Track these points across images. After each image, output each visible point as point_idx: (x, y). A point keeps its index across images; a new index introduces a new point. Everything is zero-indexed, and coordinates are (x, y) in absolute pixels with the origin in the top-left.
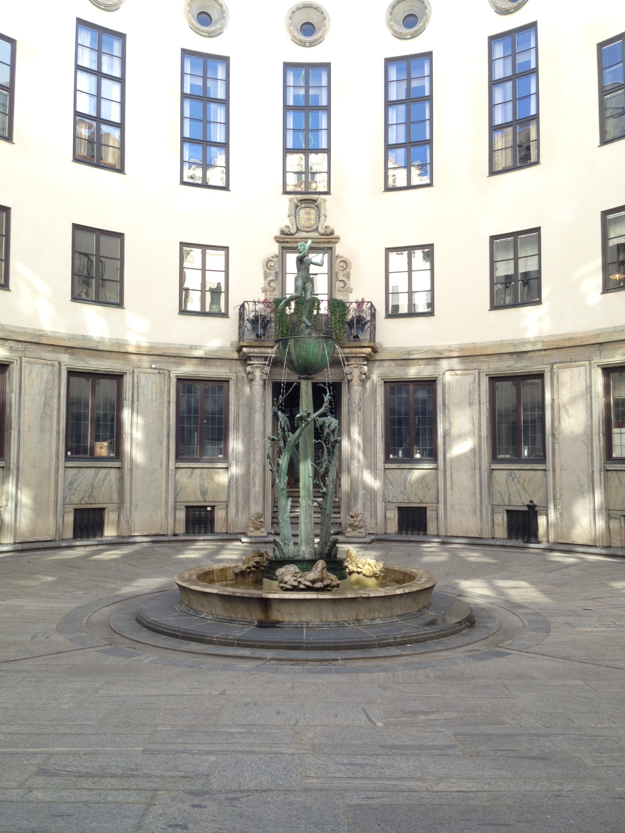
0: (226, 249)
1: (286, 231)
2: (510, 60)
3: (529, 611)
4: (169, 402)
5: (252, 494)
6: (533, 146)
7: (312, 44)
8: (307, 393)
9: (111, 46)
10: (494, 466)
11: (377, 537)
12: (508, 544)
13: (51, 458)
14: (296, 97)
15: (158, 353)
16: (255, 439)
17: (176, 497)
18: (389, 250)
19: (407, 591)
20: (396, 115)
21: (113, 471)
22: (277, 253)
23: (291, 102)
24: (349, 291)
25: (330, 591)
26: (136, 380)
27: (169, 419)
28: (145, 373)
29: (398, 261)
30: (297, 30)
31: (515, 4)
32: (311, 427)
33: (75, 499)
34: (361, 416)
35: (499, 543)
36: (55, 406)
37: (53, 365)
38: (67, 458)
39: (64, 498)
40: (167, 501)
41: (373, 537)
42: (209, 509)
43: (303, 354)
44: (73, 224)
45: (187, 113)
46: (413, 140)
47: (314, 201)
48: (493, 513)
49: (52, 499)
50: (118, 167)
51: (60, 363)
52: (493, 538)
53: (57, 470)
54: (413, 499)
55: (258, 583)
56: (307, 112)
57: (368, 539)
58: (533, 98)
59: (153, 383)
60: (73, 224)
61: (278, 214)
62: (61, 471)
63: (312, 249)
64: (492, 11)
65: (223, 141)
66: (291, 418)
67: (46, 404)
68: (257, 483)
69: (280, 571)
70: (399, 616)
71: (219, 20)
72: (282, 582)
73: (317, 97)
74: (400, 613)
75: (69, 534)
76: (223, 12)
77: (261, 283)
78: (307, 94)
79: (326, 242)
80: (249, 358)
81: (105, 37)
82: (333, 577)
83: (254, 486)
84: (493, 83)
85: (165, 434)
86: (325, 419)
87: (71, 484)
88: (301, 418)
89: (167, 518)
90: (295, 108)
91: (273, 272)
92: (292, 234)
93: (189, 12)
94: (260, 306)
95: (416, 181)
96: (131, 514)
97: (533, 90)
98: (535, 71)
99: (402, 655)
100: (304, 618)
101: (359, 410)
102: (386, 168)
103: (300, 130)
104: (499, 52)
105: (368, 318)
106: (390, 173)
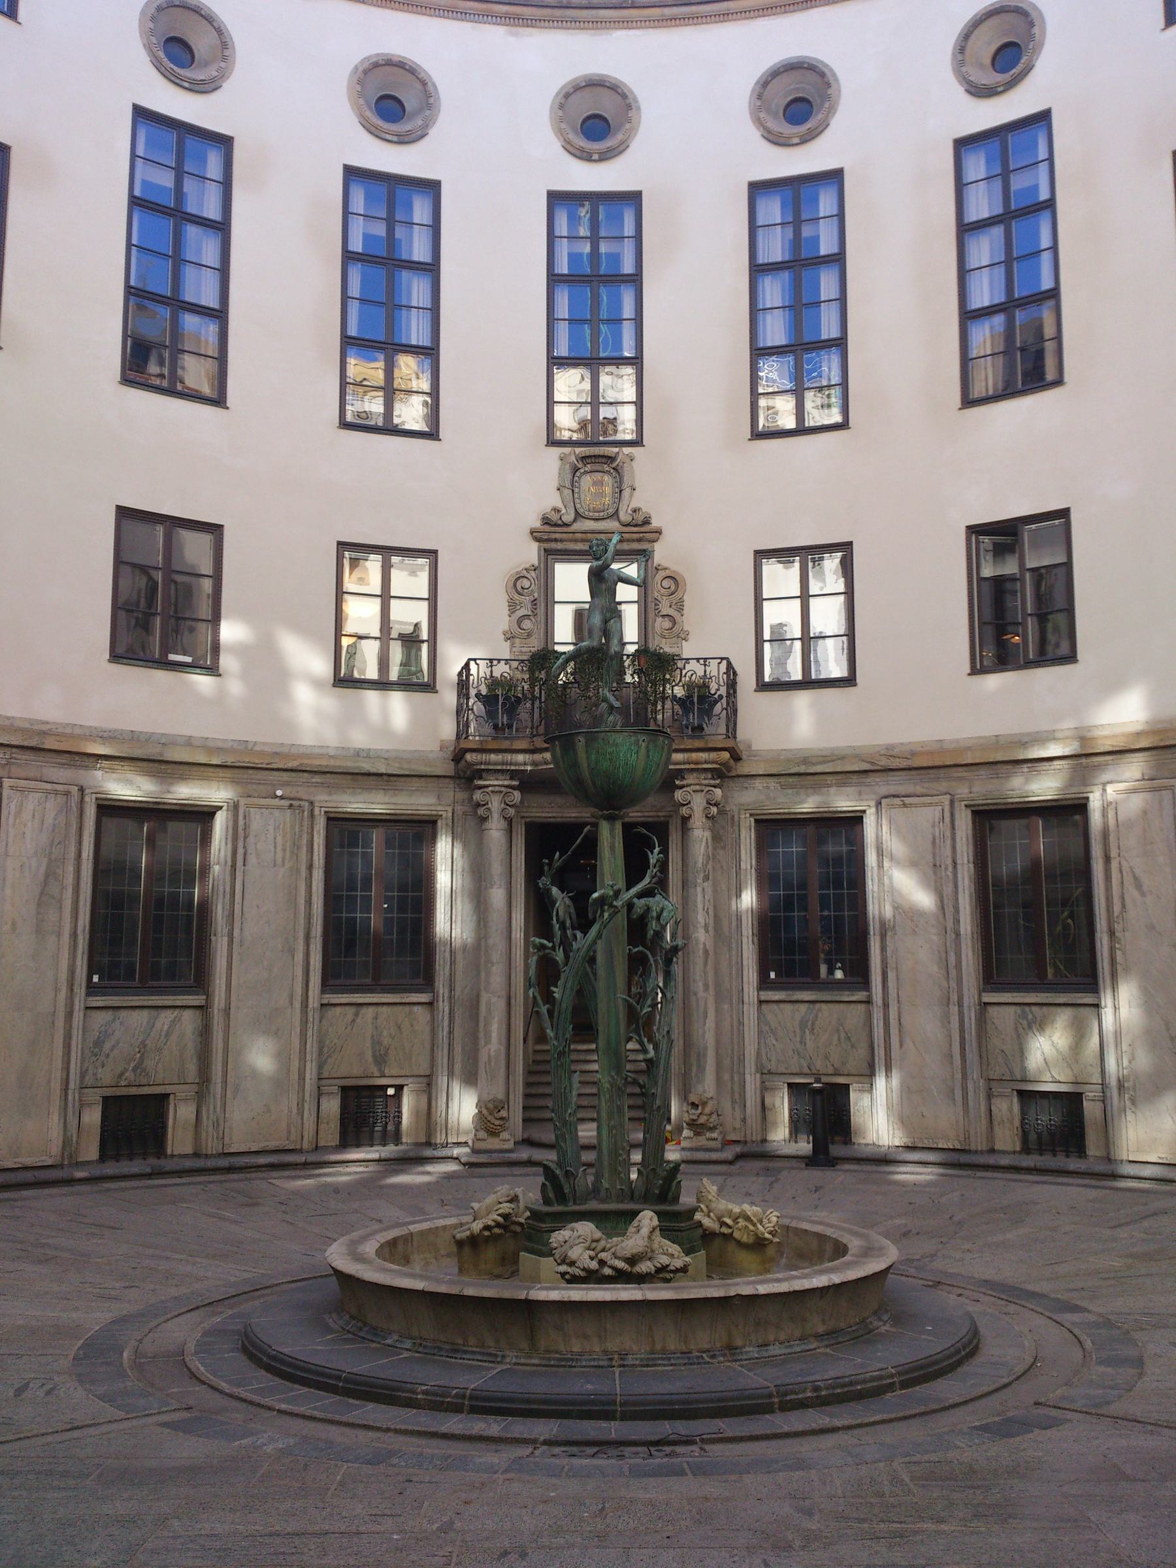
0: (431, 554)
1: (555, 517)
2: (998, 184)
3: (1092, 1318)
4: (310, 867)
5: (483, 1057)
6: (1049, 346)
7: (605, 156)
8: (612, 848)
9: (203, 161)
10: (988, 998)
11: (746, 1149)
12: (1025, 1164)
13: (57, 990)
14: (573, 258)
15: (290, 765)
16: (491, 942)
17: (320, 1067)
18: (761, 555)
19: (837, 1279)
20: (774, 291)
21: (187, 1015)
22: (536, 563)
23: (563, 268)
24: (683, 636)
25: (668, 1281)
26: (241, 822)
27: (309, 902)
28: (260, 807)
29: (781, 578)
30: (574, 129)
31: (1007, 77)
32: (621, 920)
33: (106, 1075)
34: (709, 891)
35: (1004, 1161)
36: (70, 879)
37: (67, 794)
38: (91, 989)
39: (83, 1075)
40: (302, 1078)
41: (738, 1149)
42: (391, 1091)
43: (605, 765)
44: (119, 508)
45: (355, 290)
46: (806, 340)
47: (611, 459)
48: (989, 1096)
49: (58, 1075)
50: (206, 390)
51: (82, 790)
52: (992, 1151)
53: (69, 1015)
54: (819, 1065)
55: (509, 1266)
56: (596, 282)
57: (728, 1154)
58: (1046, 257)
59: (276, 828)
60: (119, 508)
61: (537, 487)
62: (78, 1015)
63: (621, 555)
64: (959, 90)
65: (426, 342)
66: (580, 899)
67: (50, 876)
68: (494, 1035)
69: (557, 1237)
70: (817, 1336)
71: (420, 111)
72: (563, 1262)
73: (616, 258)
74: (821, 1329)
75: (91, 1152)
76: (428, 95)
77: (502, 621)
78: (595, 253)
79: (640, 537)
80: (480, 774)
81: (191, 143)
82: (675, 1249)
83: (488, 1042)
84: (965, 229)
85: (301, 935)
86: (650, 901)
87: (98, 1043)
88: (602, 900)
89: (301, 1113)
90: (570, 279)
91: (527, 600)
92: (566, 525)
93: (361, 94)
94: (500, 670)
95: (815, 417)
96: (224, 1105)
97: (1045, 242)
98: (1050, 205)
99: (834, 1430)
100: (612, 1345)
101: (706, 878)
102: (755, 395)
103: (584, 321)
104: (977, 166)
105: (723, 691)
106: (762, 402)
